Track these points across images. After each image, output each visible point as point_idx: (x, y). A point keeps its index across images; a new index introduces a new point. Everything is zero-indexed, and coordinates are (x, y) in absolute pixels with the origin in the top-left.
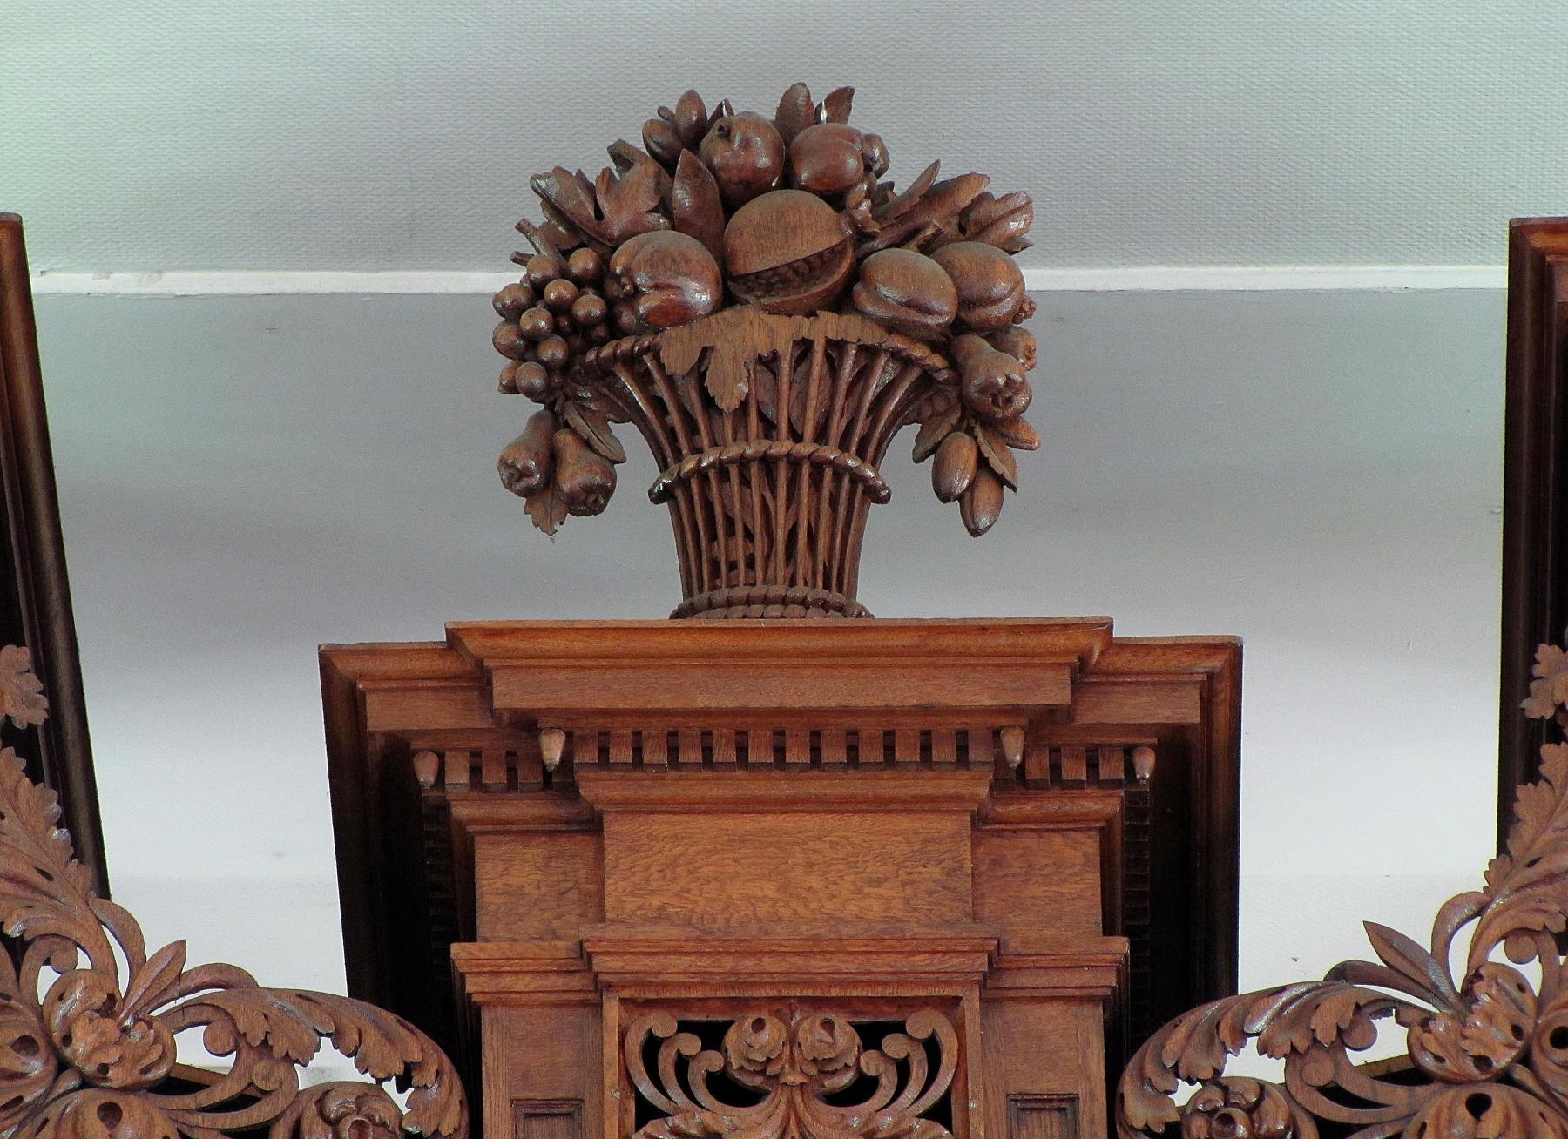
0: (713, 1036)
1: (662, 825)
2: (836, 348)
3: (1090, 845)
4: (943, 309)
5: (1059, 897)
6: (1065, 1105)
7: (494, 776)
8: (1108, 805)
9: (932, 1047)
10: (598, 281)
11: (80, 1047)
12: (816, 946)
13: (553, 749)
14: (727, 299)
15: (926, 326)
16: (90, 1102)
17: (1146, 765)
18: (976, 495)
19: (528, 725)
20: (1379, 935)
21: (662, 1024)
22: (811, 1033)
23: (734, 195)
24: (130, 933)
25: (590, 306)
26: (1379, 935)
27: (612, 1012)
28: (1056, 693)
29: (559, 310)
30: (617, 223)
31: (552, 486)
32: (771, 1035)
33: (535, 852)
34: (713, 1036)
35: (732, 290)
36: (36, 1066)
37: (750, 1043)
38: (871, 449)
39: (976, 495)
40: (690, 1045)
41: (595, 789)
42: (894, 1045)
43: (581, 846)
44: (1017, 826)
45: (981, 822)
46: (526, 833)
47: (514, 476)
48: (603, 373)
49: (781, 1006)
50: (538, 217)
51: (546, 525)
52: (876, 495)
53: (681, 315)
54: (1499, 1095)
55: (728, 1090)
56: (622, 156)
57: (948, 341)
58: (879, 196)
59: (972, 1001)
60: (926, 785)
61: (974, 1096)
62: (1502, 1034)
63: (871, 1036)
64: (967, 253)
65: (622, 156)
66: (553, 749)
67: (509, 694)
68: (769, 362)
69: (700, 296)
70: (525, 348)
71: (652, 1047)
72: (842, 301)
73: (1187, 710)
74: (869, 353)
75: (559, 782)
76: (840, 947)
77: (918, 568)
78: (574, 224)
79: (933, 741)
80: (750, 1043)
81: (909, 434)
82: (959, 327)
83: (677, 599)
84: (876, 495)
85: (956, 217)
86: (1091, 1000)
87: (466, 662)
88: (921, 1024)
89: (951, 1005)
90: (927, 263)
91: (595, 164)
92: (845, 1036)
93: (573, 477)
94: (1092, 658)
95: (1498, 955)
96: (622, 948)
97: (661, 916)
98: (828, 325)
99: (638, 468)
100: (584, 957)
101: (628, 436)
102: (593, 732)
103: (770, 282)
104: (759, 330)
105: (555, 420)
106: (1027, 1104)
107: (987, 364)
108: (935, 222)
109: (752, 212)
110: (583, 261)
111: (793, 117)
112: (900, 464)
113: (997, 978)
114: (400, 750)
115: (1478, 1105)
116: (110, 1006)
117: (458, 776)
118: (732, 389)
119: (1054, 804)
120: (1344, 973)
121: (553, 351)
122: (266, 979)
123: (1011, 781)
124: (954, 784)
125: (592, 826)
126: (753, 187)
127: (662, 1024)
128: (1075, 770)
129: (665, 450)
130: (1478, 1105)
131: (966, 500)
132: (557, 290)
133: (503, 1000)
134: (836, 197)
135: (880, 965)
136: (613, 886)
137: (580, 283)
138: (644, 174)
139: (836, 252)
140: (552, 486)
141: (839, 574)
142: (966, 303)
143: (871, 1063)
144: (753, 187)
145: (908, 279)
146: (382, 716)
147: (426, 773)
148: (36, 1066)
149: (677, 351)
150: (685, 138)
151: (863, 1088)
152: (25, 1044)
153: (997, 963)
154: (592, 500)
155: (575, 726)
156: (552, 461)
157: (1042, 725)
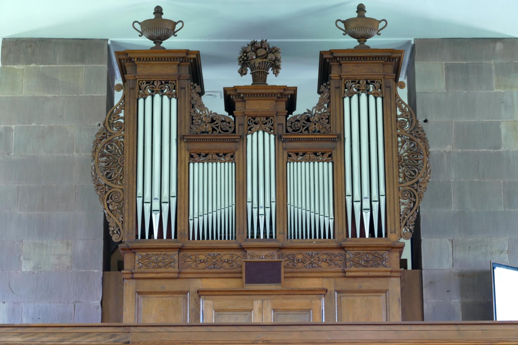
0: (254, 119)
1: (250, 101)
2: (265, 62)
3: (284, 103)
4: (274, 58)
5: (282, 106)
6: (282, 124)
7: (237, 97)
8: (286, 99)
9: (272, 120)
10: (246, 56)
11: (204, 119)
12: (262, 112)
13: (242, 95)
14: (257, 58)
15: (36, 63)
16: (204, 124)
17: (289, 96)
18: (276, 73)
19: (240, 94)
20: (308, 110)
21: (250, 118)
22: (262, 119)
23: (257, 48)
24: (208, 110)
25: (245, 58)
26: (308, 110)
27: (246, 117)
28: (282, 91)
29: (243, 59)
30: (248, 51)
31: (242, 72)
32: (259, 119)
33: (240, 103)
34: (254, 119)
35: (257, 57)
36: (200, 121)
37: (257, 119)
38: (268, 70)
39: (276, 73)
40: (252, 120)
41: (245, 99)
42: (269, 120)
43: (243, 103)
44: (279, 101)
45: (276, 101)
46: (240, 102)
47: (239, 72)
48: (246, 63)
49: (260, 117)
50: (241, 50)
51: (242, 76)
52: (268, 73)
53: (253, 59)
54: (317, 123)
55: (255, 123)
56: (248, 45)
57: (274, 61)
58: (269, 48)
59: (275, 116)
60: (272, 98)
61: (232, 255)
62: (317, 118)
63: (267, 119)
64: (276, 54)
65: (248, 45)
66: (242, 95)
67: (238, 91)
68: (260, 63)
69: (254, 57)
70: (240, 62)
71: (249, 120)
72: (266, 58)
73: (293, 92)
74: (268, 62)
75: (243, 98)
76: (264, 112)
77: (272, 80)
78: (245, 51)
79: (272, 95)
80: (257, 119)
81: (271, 68)
82: (275, 60)
83: (252, 83)
84: (268, 73)
85: (274, 51)
86: (284, 115)
87: (235, 88)
88: (271, 118)
89: (273, 116)
90: (273, 55)
91: (246, 46)
92: (265, 119)
93: (244, 72)
94: (285, 88)
95: (317, 111)
96: (247, 112)
97: (250, 109)
98: (265, 60)
99: (249, 71)
100: (244, 112)
101: (248, 68)
102: (245, 94)
103: (260, 56)
104: (259, 60)
105: (242, 67)
106: (279, 124)
107: (277, 63)
108: (274, 51)
109: (259, 50)
110: (245, 54)
111: (262, 42)
112: (270, 71)
113: (277, 114)
114: (229, 95)
115: (315, 124)
116: (206, 116)
117: (234, 97)
118: (257, 65)
119: (282, 99)
120: (305, 113)
121: (242, 62)
122: (219, 113)
123: (278, 98)
124: (274, 98)
125: (245, 101)
126: (259, 48)
127: (250, 118)
128: (284, 97)
129: (251, 70)
130: (315, 124)
131: (276, 74)
132: (243, 57)
133: (237, 116)
134: (265, 49)
135: (268, 113)
136: (246, 106)
137: (245, 56)
138: (250, 47)
139: (264, 55)
140: (242, 72)
141: (265, 81)
142: (276, 58)
143: (267, 121)
144: (259, 48)
145: (271, 56)
146: (228, 93)
147: (231, 97)
148: (200, 121)
149: (252, 62)
150: (253, 44)
151: (266, 123)
152: (199, 119)
153: (277, 113)
154: (245, 74)
155: (244, 94)
156: (242, 71)
157: (281, 94)
